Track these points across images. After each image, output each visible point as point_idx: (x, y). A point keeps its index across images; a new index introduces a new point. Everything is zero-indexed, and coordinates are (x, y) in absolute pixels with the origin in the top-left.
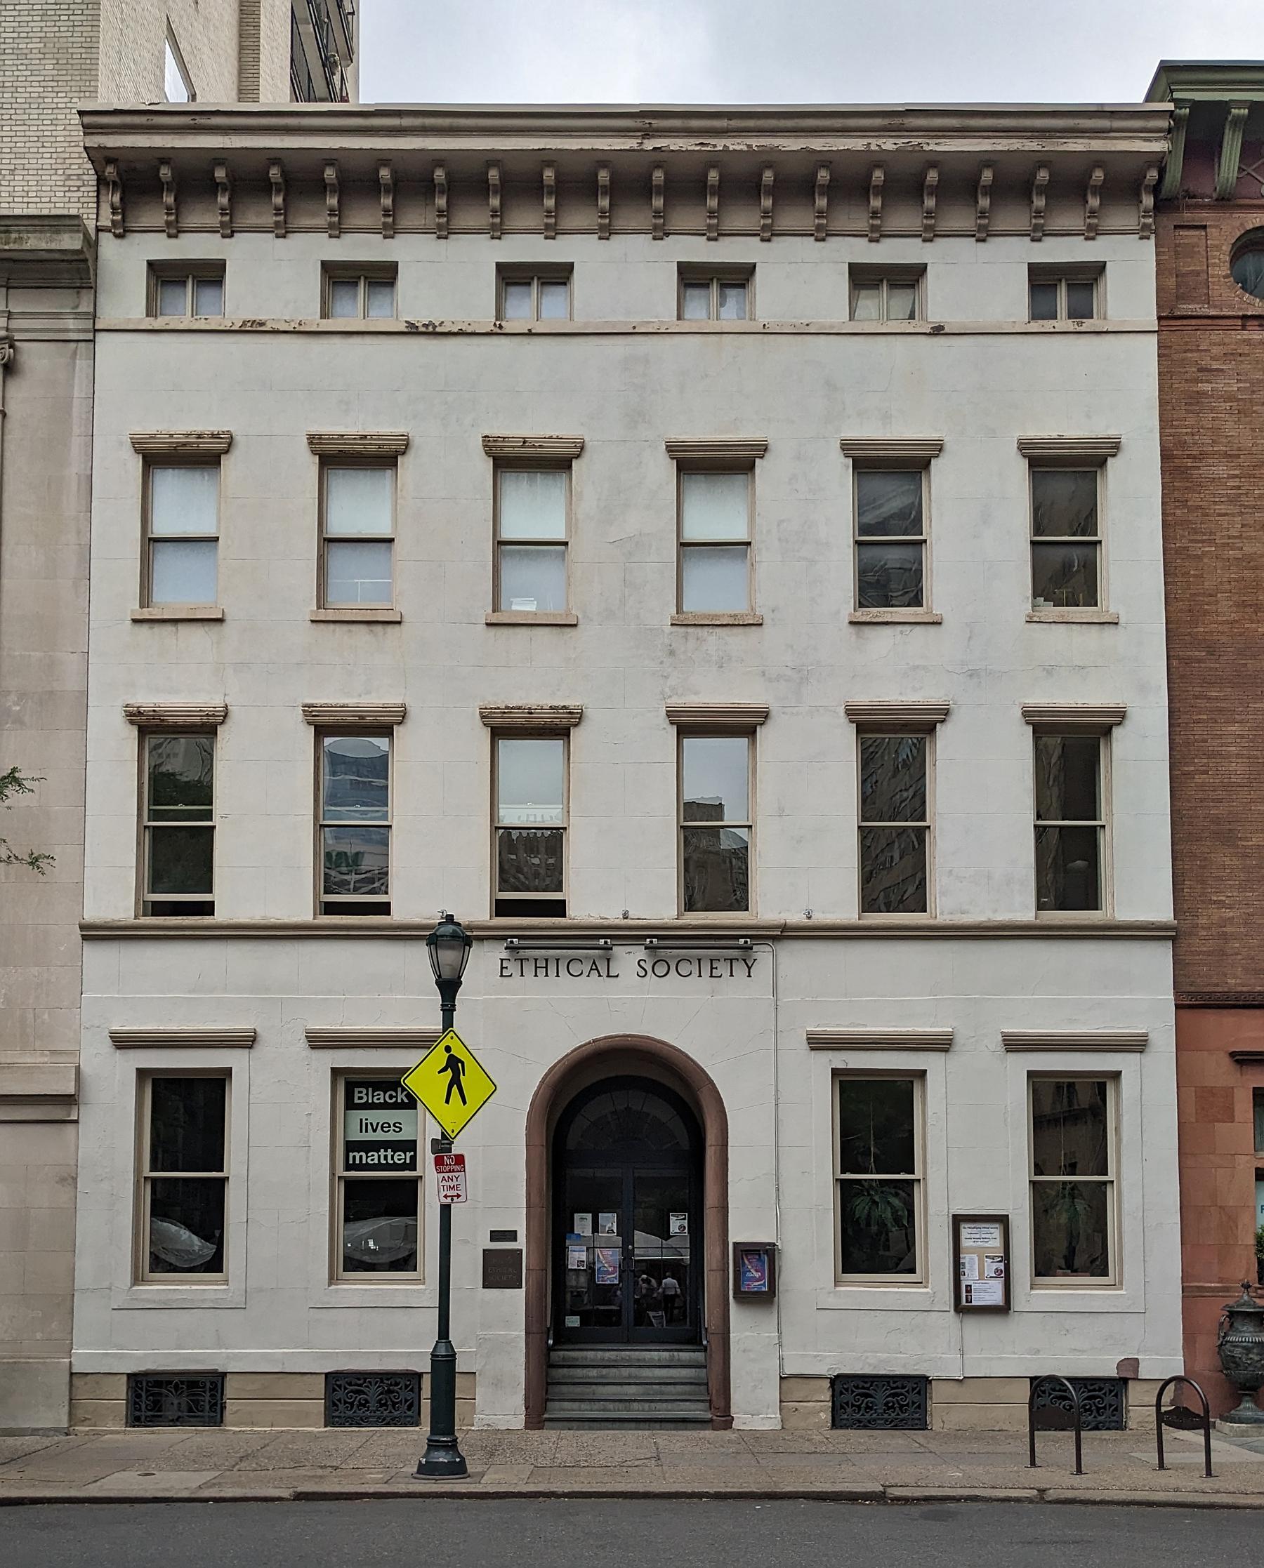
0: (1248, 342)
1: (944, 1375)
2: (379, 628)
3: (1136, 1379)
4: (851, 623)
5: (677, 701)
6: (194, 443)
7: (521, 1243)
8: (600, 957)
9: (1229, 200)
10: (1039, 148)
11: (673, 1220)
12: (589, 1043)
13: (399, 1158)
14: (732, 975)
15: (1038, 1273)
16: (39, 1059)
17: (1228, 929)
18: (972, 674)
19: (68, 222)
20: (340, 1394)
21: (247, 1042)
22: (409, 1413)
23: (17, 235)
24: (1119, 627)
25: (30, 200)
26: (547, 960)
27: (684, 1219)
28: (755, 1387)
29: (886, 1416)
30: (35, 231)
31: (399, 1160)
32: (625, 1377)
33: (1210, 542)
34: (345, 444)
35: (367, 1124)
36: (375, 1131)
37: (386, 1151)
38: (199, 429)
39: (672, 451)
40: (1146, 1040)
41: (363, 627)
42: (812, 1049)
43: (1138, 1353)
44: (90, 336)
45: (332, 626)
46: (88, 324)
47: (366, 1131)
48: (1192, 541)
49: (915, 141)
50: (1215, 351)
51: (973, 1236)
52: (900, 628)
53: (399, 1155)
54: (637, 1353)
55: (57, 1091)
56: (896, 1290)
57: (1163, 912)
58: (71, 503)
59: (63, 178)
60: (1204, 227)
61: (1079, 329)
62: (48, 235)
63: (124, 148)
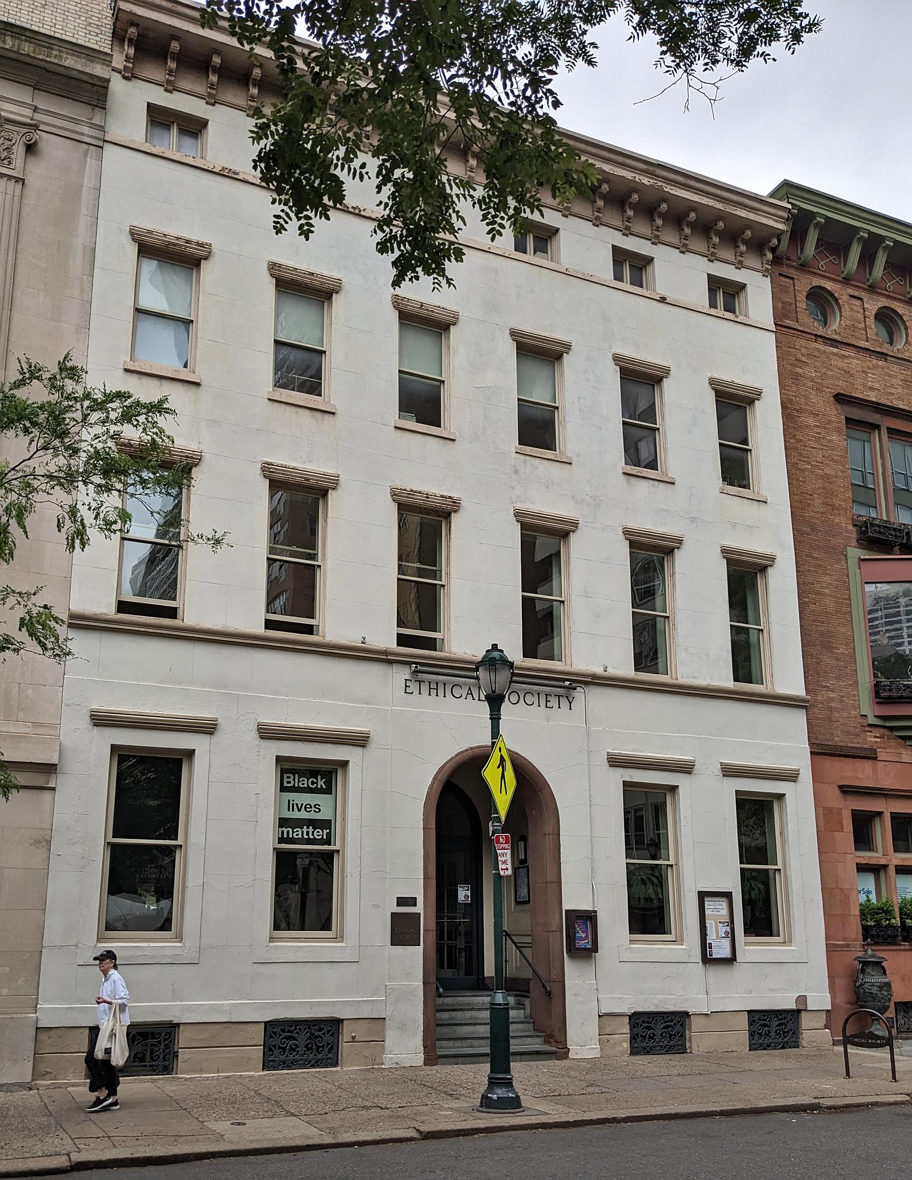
0: (818, 350)
1: (698, 1011)
2: (319, 414)
3: (806, 1010)
4: (624, 473)
5: (520, 506)
6: (184, 246)
7: (419, 908)
8: (474, 685)
9: (848, 280)
10: (723, 209)
11: (460, 890)
12: (467, 750)
13: (319, 834)
14: (559, 707)
15: (276, 927)
16: (21, 729)
17: (833, 705)
18: (693, 520)
19: (102, 57)
20: (276, 1040)
21: (208, 728)
22: (330, 1055)
23: (58, 53)
24: (768, 505)
25: (56, 30)
26: (437, 683)
27: (468, 890)
28: (583, 1023)
29: (661, 1043)
30: (74, 55)
31: (318, 835)
32: (468, 1019)
33: (809, 463)
34: (297, 275)
35: (293, 804)
36: (299, 810)
37: (308, 828)
38: (180, 234)
39: (514, 335)
40: (216, 725)
41: (307, 412)
42: (611, 766)
43: (805, 992)
44: (100, 143)
45: (283, 406)
46: (99, 134)
47: (293, 810)
48: (800, 460)
49: (660, 184)
50: (803, 351)
51: (711, 907)
52: (651, 482)
53: (318, 832)
54: (468, 998)
55: (42, 760)
56: (664, 946)
57: (795, 686)
58: (76, 267)
59: (84, 23)
60: (793, 279)
61: (736, 320)
62: (83, 61)
63: (150, 19)
